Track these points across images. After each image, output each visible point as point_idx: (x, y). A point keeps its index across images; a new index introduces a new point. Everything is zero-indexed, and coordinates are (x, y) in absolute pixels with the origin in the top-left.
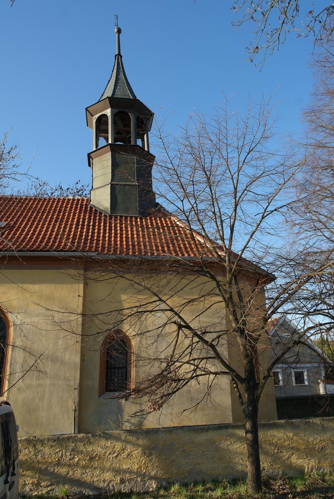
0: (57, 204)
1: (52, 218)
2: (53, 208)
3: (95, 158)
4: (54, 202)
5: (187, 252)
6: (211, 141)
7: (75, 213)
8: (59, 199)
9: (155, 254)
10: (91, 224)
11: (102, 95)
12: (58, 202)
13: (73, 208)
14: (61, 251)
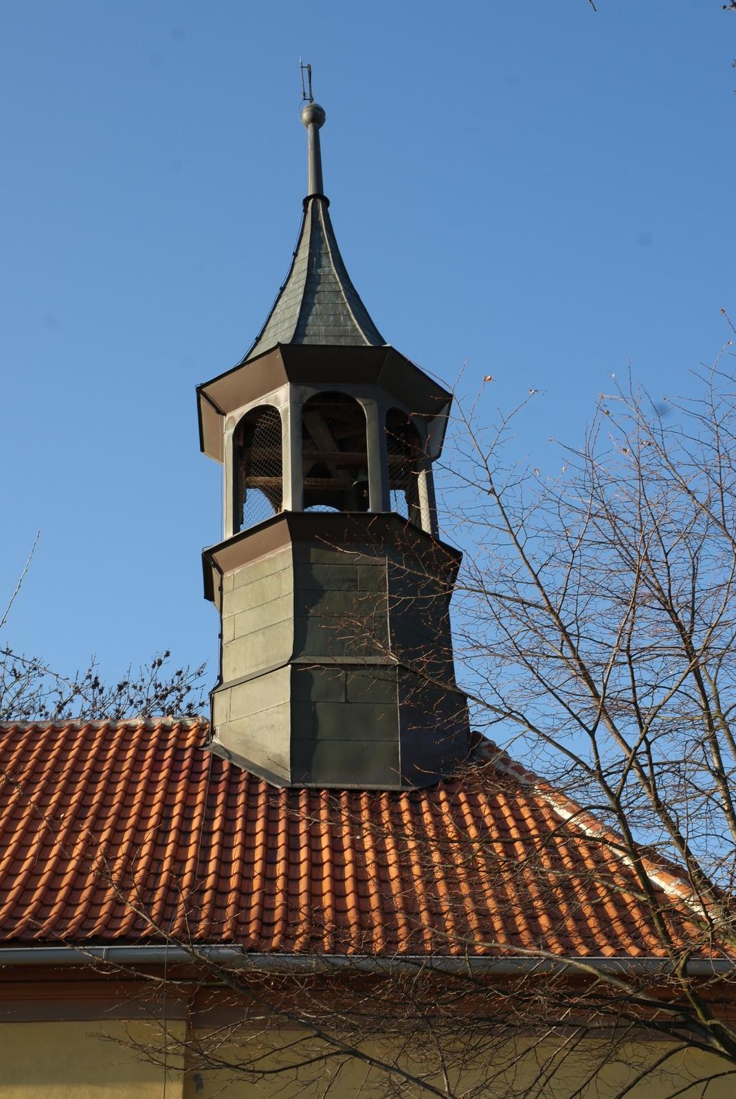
0: (84, 749)
1: (62, 805)
2: (68, 765)
3: (233, 566)
4: (69, 739)
5: (612, 938)
6: (689, 492)
7: (151, 783)
8: (91, 729)
9: (480, 949)
10: (216, 824)
11: (258, 339)
12: (88, 739)
13: (146, 764)
14: (97, 940)
